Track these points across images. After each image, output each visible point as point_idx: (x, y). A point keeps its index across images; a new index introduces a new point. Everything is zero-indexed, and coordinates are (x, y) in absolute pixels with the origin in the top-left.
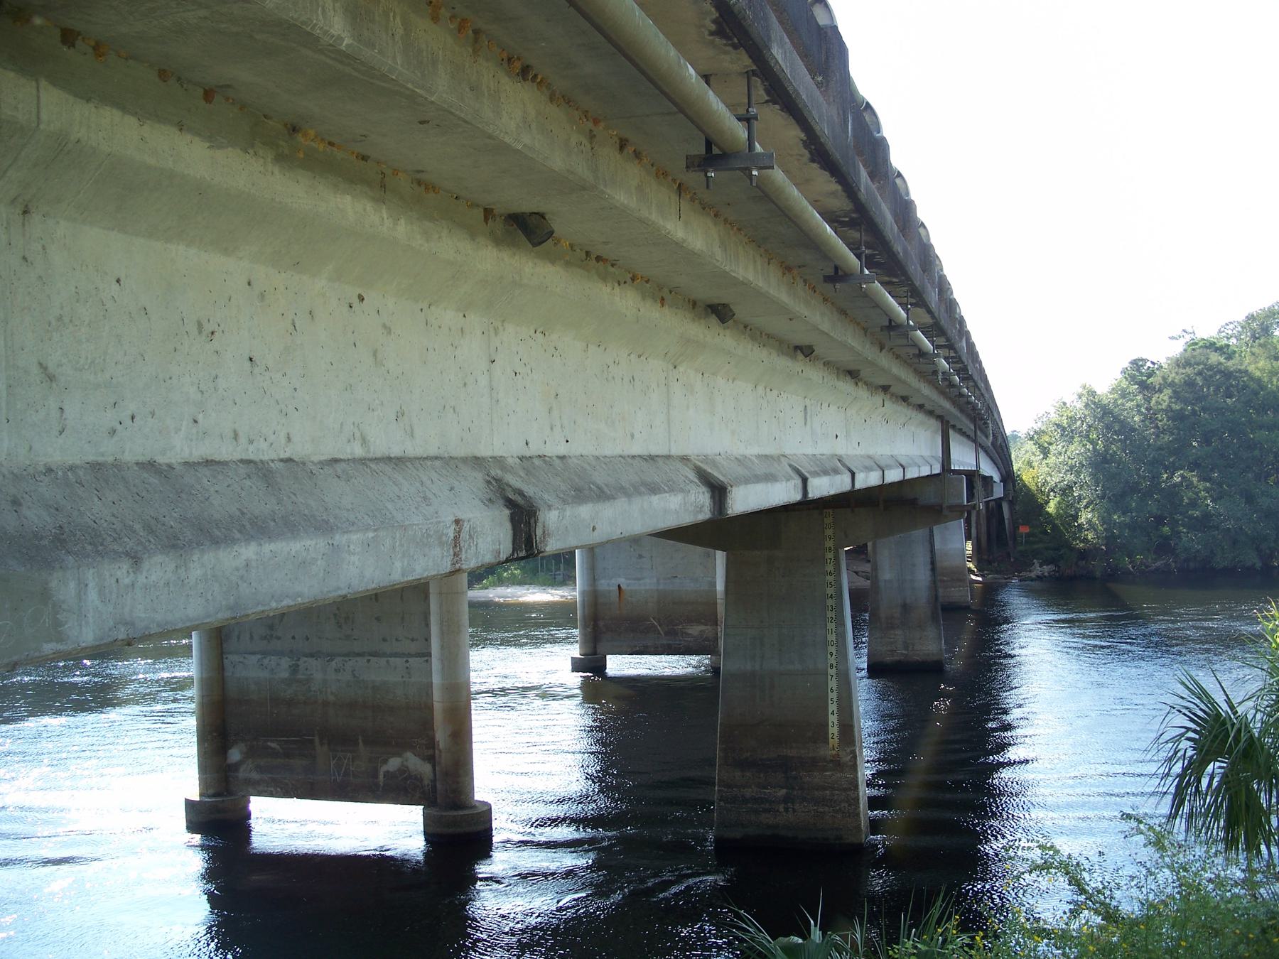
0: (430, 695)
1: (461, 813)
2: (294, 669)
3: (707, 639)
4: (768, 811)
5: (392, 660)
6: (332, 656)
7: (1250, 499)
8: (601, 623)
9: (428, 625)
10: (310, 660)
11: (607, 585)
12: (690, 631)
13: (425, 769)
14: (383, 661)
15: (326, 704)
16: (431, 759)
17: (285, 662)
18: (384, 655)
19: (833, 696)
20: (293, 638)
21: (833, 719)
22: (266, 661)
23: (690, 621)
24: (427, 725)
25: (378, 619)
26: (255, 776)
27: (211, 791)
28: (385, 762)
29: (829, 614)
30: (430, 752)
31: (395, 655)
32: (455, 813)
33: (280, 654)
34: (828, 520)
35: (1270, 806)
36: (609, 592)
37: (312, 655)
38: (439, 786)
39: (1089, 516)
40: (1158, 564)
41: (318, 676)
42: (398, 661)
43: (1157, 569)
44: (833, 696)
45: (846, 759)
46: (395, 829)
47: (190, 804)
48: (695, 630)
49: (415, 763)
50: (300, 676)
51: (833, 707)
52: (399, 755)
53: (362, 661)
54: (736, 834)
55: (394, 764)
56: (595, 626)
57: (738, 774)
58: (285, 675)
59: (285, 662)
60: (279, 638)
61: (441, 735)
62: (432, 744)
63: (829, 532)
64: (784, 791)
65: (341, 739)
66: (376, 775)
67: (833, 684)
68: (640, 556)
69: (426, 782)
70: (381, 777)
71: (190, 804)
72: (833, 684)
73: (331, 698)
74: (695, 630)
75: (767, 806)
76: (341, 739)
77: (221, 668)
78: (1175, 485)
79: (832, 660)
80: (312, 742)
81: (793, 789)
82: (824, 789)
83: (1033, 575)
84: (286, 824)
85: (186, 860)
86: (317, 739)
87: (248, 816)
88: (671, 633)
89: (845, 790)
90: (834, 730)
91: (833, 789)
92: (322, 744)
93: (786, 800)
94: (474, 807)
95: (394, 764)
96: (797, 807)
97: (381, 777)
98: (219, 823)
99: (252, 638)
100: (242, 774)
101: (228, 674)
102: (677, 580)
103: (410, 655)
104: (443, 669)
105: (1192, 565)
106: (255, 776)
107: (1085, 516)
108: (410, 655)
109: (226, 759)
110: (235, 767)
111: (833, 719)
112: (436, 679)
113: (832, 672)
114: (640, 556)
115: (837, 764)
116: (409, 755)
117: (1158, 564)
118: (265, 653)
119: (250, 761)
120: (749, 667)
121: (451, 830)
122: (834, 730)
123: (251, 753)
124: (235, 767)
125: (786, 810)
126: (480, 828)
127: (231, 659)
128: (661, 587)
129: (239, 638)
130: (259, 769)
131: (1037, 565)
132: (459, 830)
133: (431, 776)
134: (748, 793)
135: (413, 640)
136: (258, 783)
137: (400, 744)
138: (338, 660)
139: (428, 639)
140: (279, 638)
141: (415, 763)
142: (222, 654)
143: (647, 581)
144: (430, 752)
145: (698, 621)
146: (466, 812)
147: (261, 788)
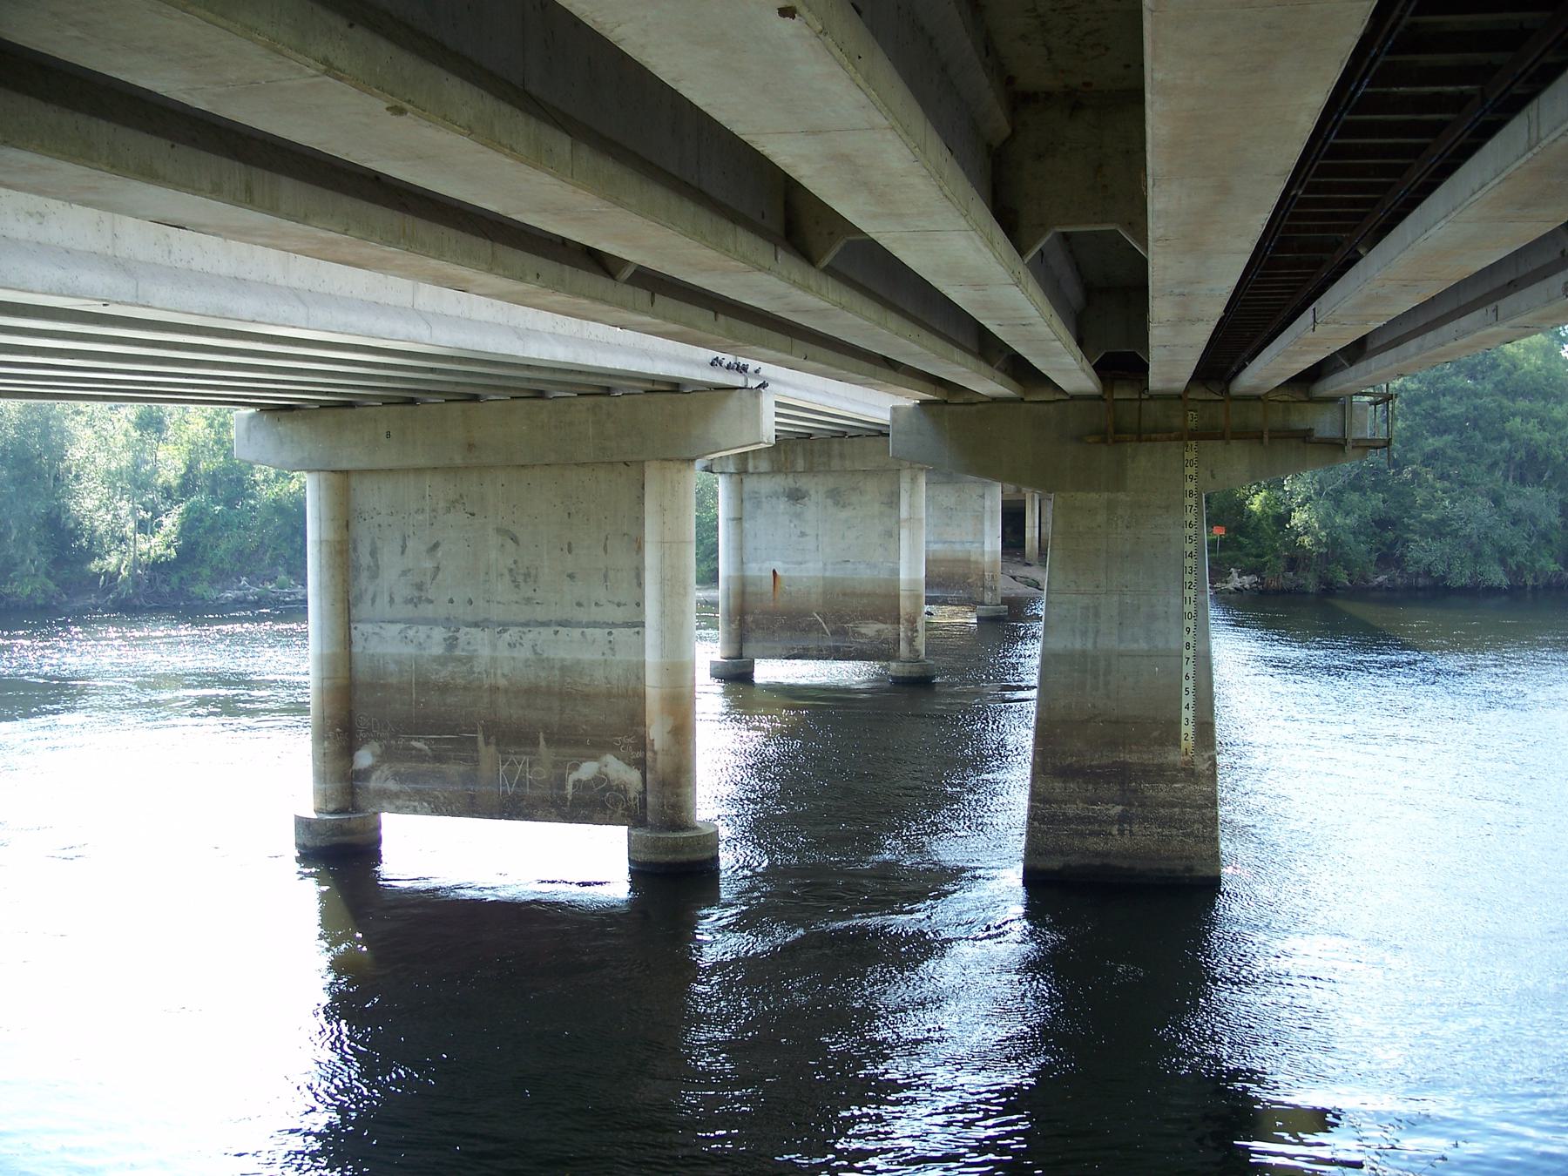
0: (641, 678)
1: (685, 835)
2: (452, 643)
3: (885, 641)
4: (1098, 834)
5: (588, 631)
6: (504, 626)
7: (1497, 500)
8: (749, 619)
9: (640, 584)
10: (473, 630)
11: (759, 570)
12: (863, 631)
13: (631, 777)
14: (576, 632)
15: (494, 689)
16: (641, 764)
17: (439, 633)
18: (579, 624)
19: (1188, 684)
20: (451, 601)
21: (1187, 714)
22: (411, 633)
23: (865, 617)
24: (635, 719)
25: (571, 576)
26: (392, 786)
27: (331, 807)
28: (576, 767)
29: (1188, 578)
30: (639, 754)
31: (595, 624)
32: (676, 835)
33: (431, 622)
34: (1190, 455)
35: (788, 993)
36: (761, 578)
37: (476, 625)
38: (649, 799)
39: (1305, 516)
40: (1380, 579)
41: (485, 652)
42: (598, 633)
43: (1380, 585)
44: (1188, 684)
45: (1203, 767)
46: (585, 863)
47: (303, 824)
48: (870, 629)
49: (618, 770)
50: (458, 653)
51: (1188, 699)
52: (595, 758)
53: (547, 633)
54: (1055, 863)
55: (587, 770)
56: (742, 622)
57: (1058, 785)
58: (438, 650)
59: (439, 633)
60: (431, 602)
61: (657, 731)
62: (642, 743)
63: (1190, 471)
64: (1120, 808)
65: (514, 738)
66: (562, 786)
67: (1188, 669)
68: (803, 534)
69: (632, 795)
70: (569, 788)
71: (303, 824)
72: (1188, 669)
73: (502, 682)
74: (870, 629)
75: (1096, 827)
76: (514, 738)
77: (348, 642)
78: (1405, 483)
79: (1189, 638)
80: (474, 740)
81: (1131, 804)
82: (1173, 805)
83: (1230, 586)
84: (426, 850)
85: (303, 898)
86: (480, 737)
87: (379, 841)
88: (840, 632)
89: (1200, 807)
90: (1187, 729)
91: (1184, 805)
92: (487, 743)
93: (1123, 819)
94: (695, 828)
95: (587, 770)
96: (1135, 828)
97: (569, 788)
98: (340, 854)
99: (392, 600)
100: (374, 784)
101: (357, 649)
102: (849, 565)
103: (614, 625)
104: (663, 643)
105: (1421, 581)
106: (392, 786)
107: (1299, 518)
108: (614, 625)
109: (352, 762)
110: (365, 774)
111: (1187, 714)
112: (652, 657)
113: (1190, 653)
114: (803, 534)
115: (1190, 773)
116: (610, 758)
117: (1380, 579)
118: (410, 622)
119: (385, 767)
120: (1078, 646)
121: (669, 858)
122: (1187, 729)
123: (386, 756)
124: (365, 774)
125: (1121, 832)
126: (707, 855)
127: (360, 630)
128: (828, 574)
129: (373, 601)
130: (397, 776)
131: (1235, 575)
132: (683, 858)
133: (640, 787)
134: (1071, 810)
135: (619, 605)
136: (397, 795)
137: (599, 744)
138: (513, 631)
139: (639, 604)
140: (431, 602)
141: (618, 770)
142: (349, 622)
143: (810, 565)
144: (639, 754)
145: (876, 618)
146: (685, 835)
147: (399, 803)
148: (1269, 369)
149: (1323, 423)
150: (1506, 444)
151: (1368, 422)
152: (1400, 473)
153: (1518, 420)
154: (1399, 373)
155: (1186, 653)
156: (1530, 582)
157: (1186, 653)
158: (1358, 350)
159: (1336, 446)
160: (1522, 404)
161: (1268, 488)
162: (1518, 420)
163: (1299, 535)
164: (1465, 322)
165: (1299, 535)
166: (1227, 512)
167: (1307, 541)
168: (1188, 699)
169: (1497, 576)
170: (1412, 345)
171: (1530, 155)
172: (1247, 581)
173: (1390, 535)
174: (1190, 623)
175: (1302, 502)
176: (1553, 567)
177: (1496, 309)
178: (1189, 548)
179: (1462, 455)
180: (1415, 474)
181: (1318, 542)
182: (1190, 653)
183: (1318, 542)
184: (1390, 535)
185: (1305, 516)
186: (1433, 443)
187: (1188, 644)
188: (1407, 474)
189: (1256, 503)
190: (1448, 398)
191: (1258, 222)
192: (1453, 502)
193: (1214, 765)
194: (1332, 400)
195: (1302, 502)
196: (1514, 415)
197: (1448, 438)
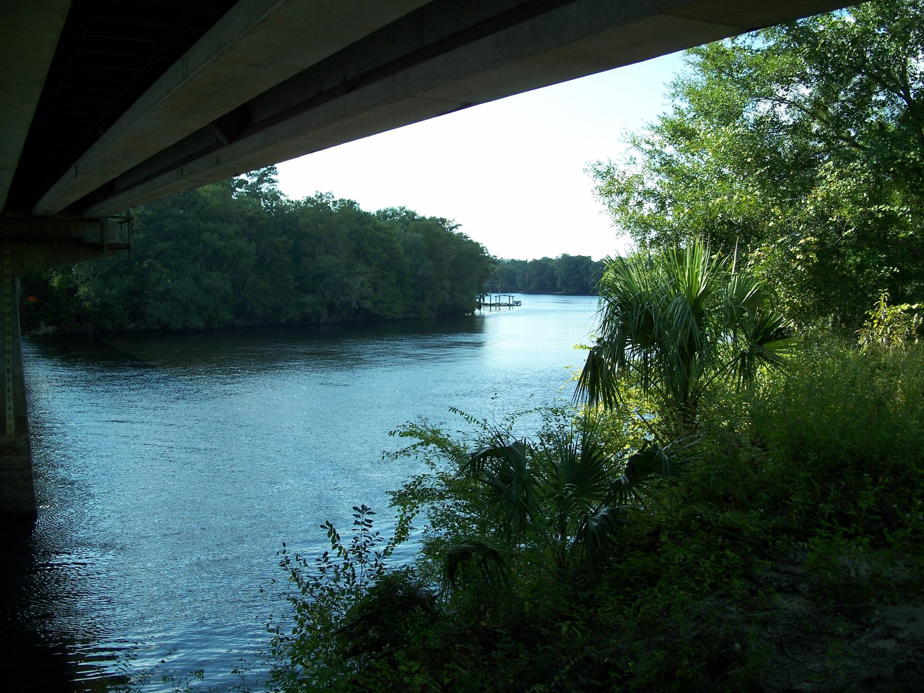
7: (197, 279)
39: (86, 289)
40: (132, 326)
44: (10, 394)
67: (9, 385)
72: (9, 385)
83: (40, 333)
90: (10, 422)
107: (83, 290)
111: (10, 413)
113: (10, 375)
117: (132, 326)
122: (10, 422)
148: (56, 199)
149: (90, 234)
150: (201, 246)
151: (116, 234)
152: (142, 263)
153: (208, 234)
154: (139, 206)
155: (7, 375)
156: (216, 326)
157: (7, 375)
158: (108, 190)
159: (98, 248)
160: (211, 225)
161: (62, 272)
162: (208, 234)
163: (83, 301)
164: (165, 177)
165: (83, 301)
166: (36, 286)
167: (87, 304)
168: (10, 404)
169: (197, 322)
170: (138, 189)
171: (183, 83)
172: (51, 329)
173: (136, 300)
174: (9, 357)
175: (83, 280)
176: (228, 317)
177: (182, 171)
178: (7, 310)
179: (625, 195)
180: (150, 264)
181: (95, 305)
182: (10, 375)
183: (95, 305)
184: (136, 300)
185: (86, 289)
186: (160, 246)
187: (8, 370)
188: (145, 265)
189: (55, 282)
190: (169, 220)
191: (29, 110)
192: (173, 281)
193: (28, 443)
194: (95, 220)
195: (83, 280)
196: (205, 231)
197: (170, 243)
